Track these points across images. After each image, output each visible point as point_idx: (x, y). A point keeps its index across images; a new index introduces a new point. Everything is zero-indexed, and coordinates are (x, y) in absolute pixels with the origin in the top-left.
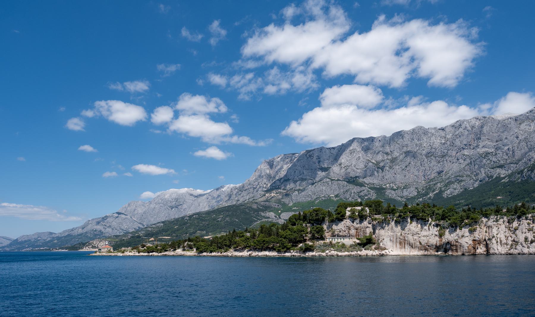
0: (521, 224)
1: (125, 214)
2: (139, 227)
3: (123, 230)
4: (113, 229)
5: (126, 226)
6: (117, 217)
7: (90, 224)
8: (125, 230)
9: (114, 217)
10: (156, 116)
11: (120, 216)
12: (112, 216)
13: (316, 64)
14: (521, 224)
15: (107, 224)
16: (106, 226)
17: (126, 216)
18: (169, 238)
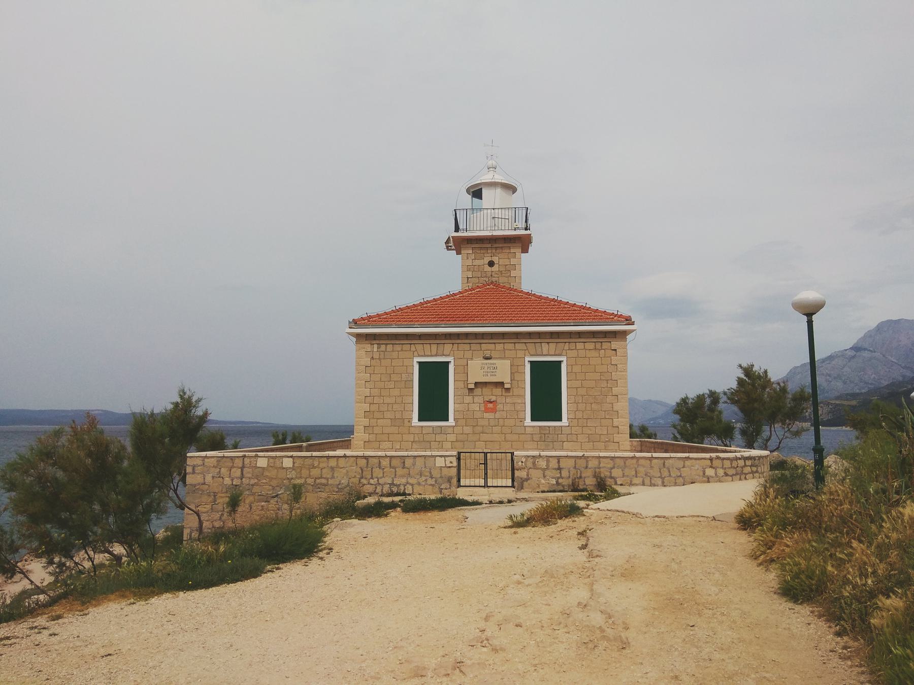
0: (843, 502)
1: (869, 350)
2: (904, 376)
3: (866, 383)
4: (845, 383)
5: (873, 375)
6: (854, 357)
7: (799, 373)
8: (871, 384)
9: (847, 356)
10: (199, 400)
11: (858, 354)
12: (842, 355)
13: (351, 321)
14: (843, 502)
15: (832, 372)
16: (829, 375)
17: (874, 353)
18: (903, 399)
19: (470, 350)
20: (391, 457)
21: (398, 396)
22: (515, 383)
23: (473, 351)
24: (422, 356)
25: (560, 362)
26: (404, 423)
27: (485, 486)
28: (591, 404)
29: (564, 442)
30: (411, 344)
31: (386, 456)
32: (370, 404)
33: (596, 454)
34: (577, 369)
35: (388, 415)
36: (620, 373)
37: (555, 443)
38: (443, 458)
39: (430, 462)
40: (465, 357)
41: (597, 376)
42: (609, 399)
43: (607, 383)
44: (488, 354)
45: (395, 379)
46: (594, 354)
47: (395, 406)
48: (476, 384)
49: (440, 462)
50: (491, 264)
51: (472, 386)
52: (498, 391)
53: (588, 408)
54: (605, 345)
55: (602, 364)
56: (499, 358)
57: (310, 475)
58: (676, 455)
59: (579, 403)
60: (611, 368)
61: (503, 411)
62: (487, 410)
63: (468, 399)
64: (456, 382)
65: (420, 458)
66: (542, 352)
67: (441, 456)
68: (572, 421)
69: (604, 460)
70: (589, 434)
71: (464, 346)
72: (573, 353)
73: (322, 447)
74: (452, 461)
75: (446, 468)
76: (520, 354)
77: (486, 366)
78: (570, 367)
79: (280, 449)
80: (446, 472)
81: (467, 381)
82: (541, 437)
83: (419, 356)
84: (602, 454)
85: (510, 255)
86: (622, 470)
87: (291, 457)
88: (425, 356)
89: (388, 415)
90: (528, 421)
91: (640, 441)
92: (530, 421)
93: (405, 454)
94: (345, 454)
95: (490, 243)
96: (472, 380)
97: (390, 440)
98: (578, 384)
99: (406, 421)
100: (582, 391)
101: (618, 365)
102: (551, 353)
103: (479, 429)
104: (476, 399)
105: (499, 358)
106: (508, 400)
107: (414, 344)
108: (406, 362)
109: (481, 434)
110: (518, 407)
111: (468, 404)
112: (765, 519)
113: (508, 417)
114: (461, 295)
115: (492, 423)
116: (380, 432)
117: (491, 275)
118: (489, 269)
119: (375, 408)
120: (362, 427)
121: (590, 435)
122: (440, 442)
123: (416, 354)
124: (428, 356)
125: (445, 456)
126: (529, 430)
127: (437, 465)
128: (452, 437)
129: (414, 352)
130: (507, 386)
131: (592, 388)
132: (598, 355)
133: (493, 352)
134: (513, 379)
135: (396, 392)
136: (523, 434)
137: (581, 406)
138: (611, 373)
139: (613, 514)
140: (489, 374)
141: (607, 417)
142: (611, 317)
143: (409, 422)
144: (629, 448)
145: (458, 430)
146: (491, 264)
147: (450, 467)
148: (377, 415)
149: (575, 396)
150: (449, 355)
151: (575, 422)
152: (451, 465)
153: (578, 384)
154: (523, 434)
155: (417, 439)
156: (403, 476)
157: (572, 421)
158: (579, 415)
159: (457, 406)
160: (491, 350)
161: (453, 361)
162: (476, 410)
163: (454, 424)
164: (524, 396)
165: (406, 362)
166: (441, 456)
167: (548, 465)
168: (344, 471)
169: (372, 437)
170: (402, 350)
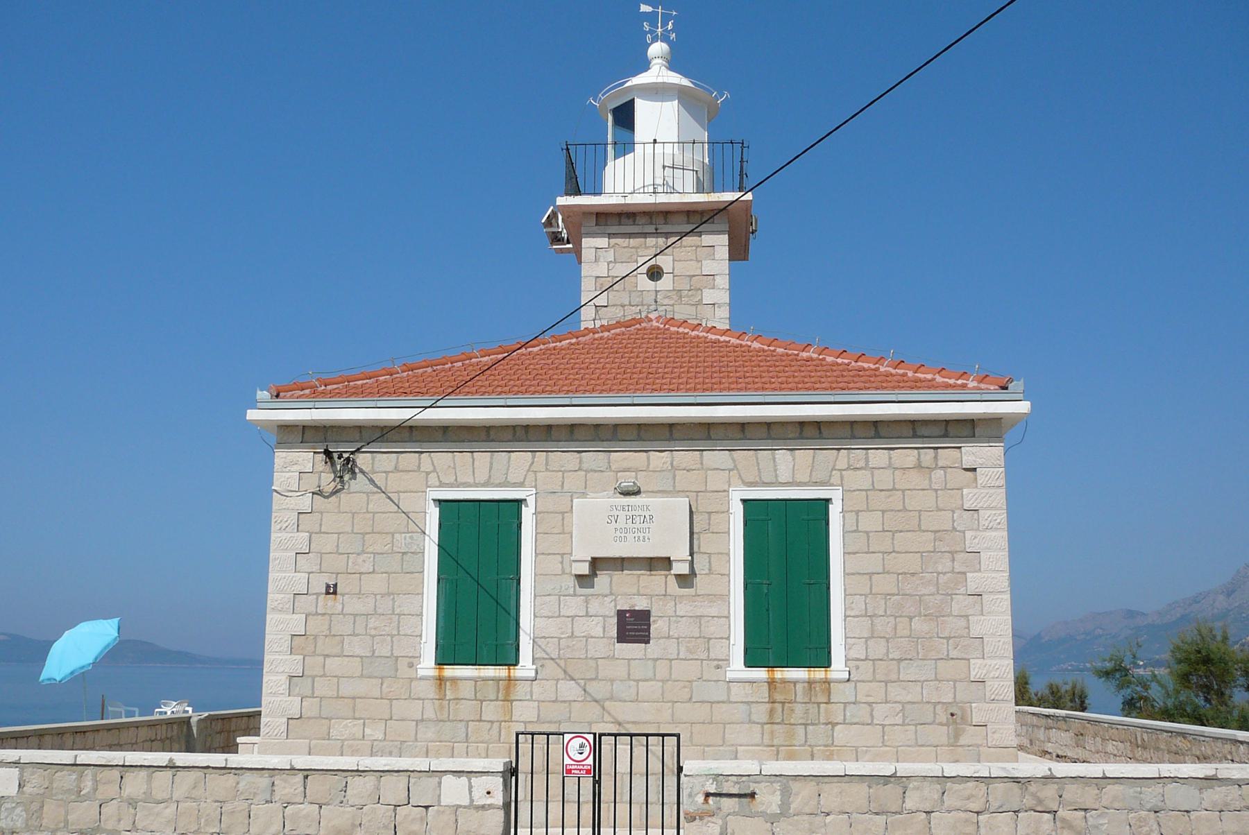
19: (580, 469)
20: (307, 773)
21: (383, 596)
24: (451, 485)
25: (828, 501)
26: (397, 670)
28: (911, 619)
29: (837, 724)
31: (293, 769)
33: (932, 768)
34: (870, 522)
35: (356, 647)
36: (988, 534)
37: (810, 728)
38: (464, 779)
40: (566, 488)
42: (959, 604)
43: (953, 560)
44: (627, 482)
45: (378, 548)
46: (916, 479)
47: (373, 622)
49: (453, 791)
50: (655, 274)
52: (656, 581)
54: (946, 456)
55: (939, 510)
56: (656, 492)
57: (66, 822)
58: (1178, 770)
59: (875, 615)
60: (963, 520)
61: (669, 637)
63: (573, 605)
66: (776, 476)
68: (857, 668)
69: (957, 787)
70: (903, 704)
71: (564, 459)
72: (860, 480)
73: (125, 736)
75: (473, 811)
76: (716, 481)
78: (851, 517)
82: (772, 712)
83: (442, 485)
84: (951, 769)
86: (324, 434)
87: (16, 763)
88: (457, 484)
89: (356, 647)
92: (618, 608)
94: (171, 760)
95: (651, 224)
96: (583, 552)
97: (357, 715)
99: (402, 664)
100: (885, 584)
102: (799, 478)
105: (656, 492)
110: (712, 628)
111: (573, 617)
113: (681, 657)
114: (574, 340)
116: (330, 694)
118: (650, 285)
120: (283, 678)
121: (908, 706)
122: (492, 722)
123: (433, 479)
126: (737, 692)
129: (428, 473)
131: (913, 574)
132: (926, 484)
133: (641, 474)
135: (376, 584)
136: (723, 702)
138: (964, 532)
139: (662, 467)
141: (954, 654)
142: (960, 382)
146: (655, 274)
147: (483, 807)
149: (866, 596)
150: (521, 485)
151: (866, 669)
152: (489, 801)
154: (723, 702)
155: (430, 714)
157: (857, 668)
158: (878, 649)
159: (541, 622)
160: (637, 471)
161: (531, 501)
163: (532, 674)
164: (725, 598)
167: (785, 805)
168: (170, 811)
169: (311, 707)
170: (397, 469)
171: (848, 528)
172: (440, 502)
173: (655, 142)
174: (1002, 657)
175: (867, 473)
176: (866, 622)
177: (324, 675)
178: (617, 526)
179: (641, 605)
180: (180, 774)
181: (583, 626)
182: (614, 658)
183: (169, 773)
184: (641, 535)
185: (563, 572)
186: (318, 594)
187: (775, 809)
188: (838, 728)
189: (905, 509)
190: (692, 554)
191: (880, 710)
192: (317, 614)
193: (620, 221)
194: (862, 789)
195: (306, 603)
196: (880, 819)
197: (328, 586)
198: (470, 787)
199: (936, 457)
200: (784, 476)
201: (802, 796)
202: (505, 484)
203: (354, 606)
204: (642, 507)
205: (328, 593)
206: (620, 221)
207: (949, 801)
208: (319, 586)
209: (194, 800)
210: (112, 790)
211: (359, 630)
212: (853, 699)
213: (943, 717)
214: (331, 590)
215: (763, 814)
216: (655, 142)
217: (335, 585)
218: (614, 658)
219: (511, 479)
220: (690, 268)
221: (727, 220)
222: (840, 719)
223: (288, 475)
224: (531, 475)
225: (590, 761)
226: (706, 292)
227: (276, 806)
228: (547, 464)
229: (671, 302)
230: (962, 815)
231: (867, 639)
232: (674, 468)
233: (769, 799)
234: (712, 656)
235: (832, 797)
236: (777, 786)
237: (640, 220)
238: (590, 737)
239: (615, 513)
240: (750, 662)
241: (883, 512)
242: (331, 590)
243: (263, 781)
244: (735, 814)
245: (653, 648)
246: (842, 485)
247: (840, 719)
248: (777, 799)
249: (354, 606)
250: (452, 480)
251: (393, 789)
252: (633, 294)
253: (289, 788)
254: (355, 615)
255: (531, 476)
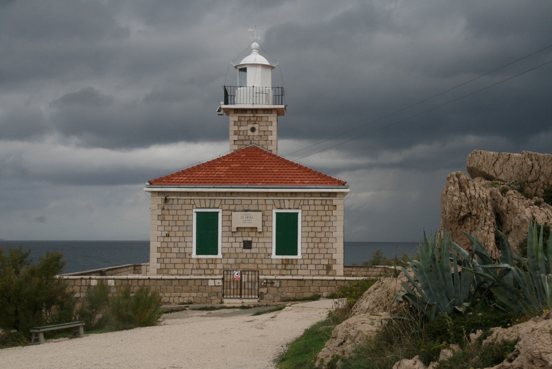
20: (179, 280)
22: (265, 228)
23: (236, 205)
26: (186, 256)
27: (240, 298)
30: (191, 199)
32: (161, 242)
34: (309, 218)
35: (175, 250)
38: (213, 280)
39: (204, 283)
41: (322, 224)
42: (331, 240)
48: (238, 228)
49: (211, 283)
50: (253, 130)
51: (235, 230)
53: (316, 246)
62: (250, 242)
64: (223, 227)
65: (198, 280)
67: (212, 279)
74: (219, 282)
77: (245, 216)
78: (304, 217)
79: (93, 273)
80: (215, 289)
81: (231, 226)
83: (197, 208)
85: (268, 124)
87: (114, 279)
89: (175, 250)
90: (274, 256)
91: (384, 267)
93: (188, 277)
94: (149, 277)
98: (309, 229)
99: (187, 255)
100: (312, 235)
101: (337, 217)
103: (239, 261)
104: (238, 239)
106: (261, 240)
107: (193, 199)
108: (188, 212)
109: (241, 264)
110: (267, 245)
111: (232, 242)
112: (427, 323)
115: (249, 256)
117: (253, 139)
119: (165, 245)
124: (203, 208)
125: (215, 279)
126: (274, 262)
127: (209, 285)
128: (220, 266)
129: (193, 205)
130: (260, 230)
134: (264, 225)
137: (311, 245)
140: (247, 222)
143: (189, 255)
144: (342, 274)
145: (224, 261)
146: (253, 130)
148: (166, 250)
150: (218, 208)
151: (306, 256)
153: (309, 229)
156: (187, 292)
157: (304, 255)
158: (309, 251)
161: (221, 212)
162: (237, 247)
165: (188, 212)
166: (212, 279)
167: (280, 285)
171: (303, 220)
172: (197, 213)
173: (253, 87)
174: (341, 253)
175: (308, 206)
176: (307, 244)
177: (167, 258)
178: (244, 219)
179: (250, 239)
180: (151, 280)
181: (235, 245)
182: (242, 253)
183: (148, 280)
184: (250, 222)
185: (229, 231)
186: (164, 237)
187: (278, 286)
188: (299, 270)
189: (318, 216)
190: (262, 226)
191: (310, 267)
192: (164, 242)
193: (242, 112)
194: (296, 282)
195: (161, 239)
196: (300, 288)
197: (167, 235)
198: (215, 282)
199: (326, 202)
200: (287, 206)
201: (284, 283)
202: (214, 208)
203: (174, 239)
204: (249, 214)
205: (167, 236)
206: (242, 112)
207: (314, 284)
208: (164, 234)
209: (154, 286)
210: (136, 284)
211: (176, 246)
212: (303, 263)
213: (325, 268)
214: (168, 236)
215: (276, 287)
216: (253, 87)
217: (169, 234)
218: (242, 253)
219: (215, 206)
220: (265, 128)
221: (276, 113)
222: (299, 268)
223: (155, 205)
224: (221, 206)
225: (240, 276)
226: (269, 137)
227: (173, 287)
228: (225, 203)
229: (258, 139)
230: (316, 287)
231: (307, 248)
232: (279, 96)
233: (277, 284)
234: (268, 252)
235: (290, 283)
236: (278, 281)
237: (248, 112)
238: (240, 272)
239: (243, 216)
240: (277, 254)
241: (312, 216)
242: (168, 236)
243: (170, 282)
244: (270, 287)
245: (253, 251)
246: (302, 209)
247: (299, 268)
248: (278, 284)
249: (174, 239)
250: (200, 207)
251: (198, 283)
252: (246, 137)
253: (174, 283)
254: (174, 242)
255: (221, 206)
